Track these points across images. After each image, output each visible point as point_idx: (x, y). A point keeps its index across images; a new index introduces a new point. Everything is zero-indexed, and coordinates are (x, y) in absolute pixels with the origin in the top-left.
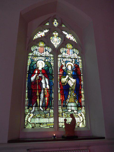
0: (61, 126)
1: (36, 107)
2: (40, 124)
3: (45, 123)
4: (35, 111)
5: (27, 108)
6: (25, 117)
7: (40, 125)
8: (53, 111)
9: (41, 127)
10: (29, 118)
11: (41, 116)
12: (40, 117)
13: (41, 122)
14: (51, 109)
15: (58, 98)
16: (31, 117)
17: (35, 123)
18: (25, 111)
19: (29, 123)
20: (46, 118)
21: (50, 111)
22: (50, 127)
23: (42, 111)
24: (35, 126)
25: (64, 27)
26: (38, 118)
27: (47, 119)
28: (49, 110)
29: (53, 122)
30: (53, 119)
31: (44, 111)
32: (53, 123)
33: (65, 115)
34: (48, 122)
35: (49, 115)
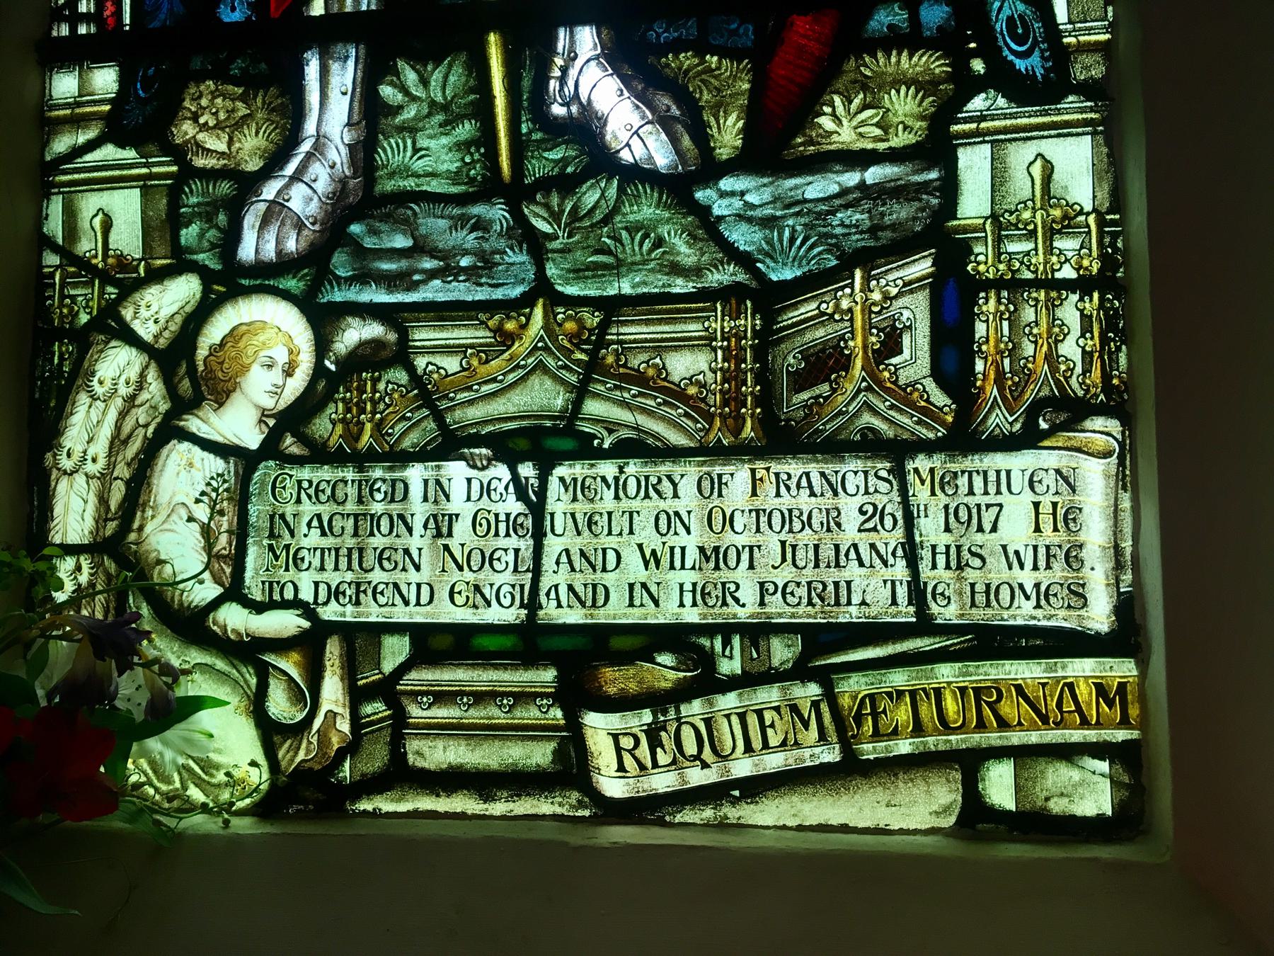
1: (424, 57)
2: (583, 662)
3: (782, 652)
4: (366, 195)
5: (120, 124)
6: (44, 429)
7: (578, 695)
8: (1075, 164)
9: (613, 787)
10: (177, 455)
11: (593, 368)
12: (543, 396)
13: (616, 612)
14: (1023, 91)
15: (316, 345)
16: (238, 423)
17: (395, 651)
18: (55, 226)
19: (192, 626)
20: (781, 439)
21: (974, 164)
22: (975, 811)
23: (646, 210)
24: (375, 759)
25: (88, 35)
26: (506, 446)
27: (852, 469)
28: (938, 148)
29: (1099, 616)
30: (1095, 478)
31: (711, 170)
32: (1082, 668)
34: (875, 591)
35: (916, 312)
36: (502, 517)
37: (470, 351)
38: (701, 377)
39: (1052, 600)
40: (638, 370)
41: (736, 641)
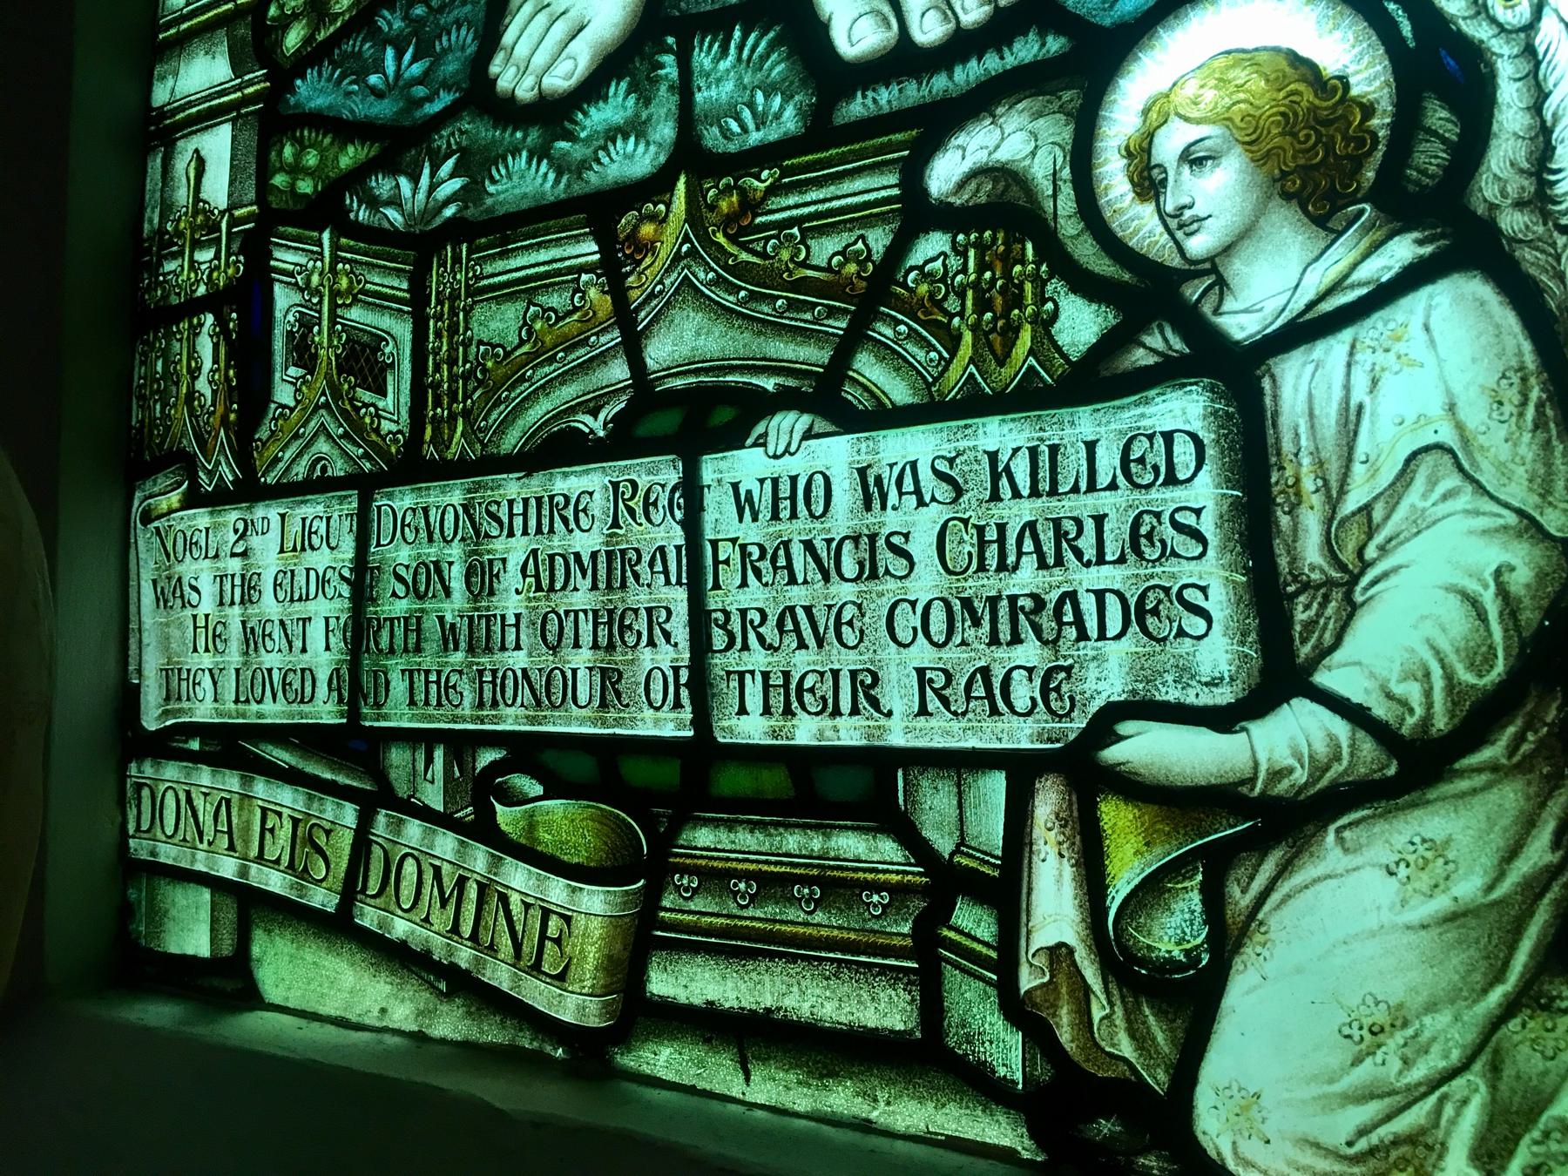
0: (192, 932)
33: (363, 361)
36: (991, 534)
37: (584, 277)
38: (938, 264)
39: (807, 697)
40: (829, 269)
41: (439, 754)
